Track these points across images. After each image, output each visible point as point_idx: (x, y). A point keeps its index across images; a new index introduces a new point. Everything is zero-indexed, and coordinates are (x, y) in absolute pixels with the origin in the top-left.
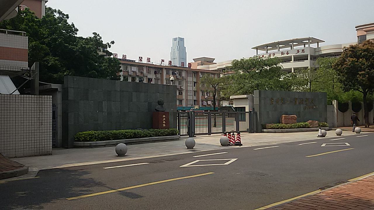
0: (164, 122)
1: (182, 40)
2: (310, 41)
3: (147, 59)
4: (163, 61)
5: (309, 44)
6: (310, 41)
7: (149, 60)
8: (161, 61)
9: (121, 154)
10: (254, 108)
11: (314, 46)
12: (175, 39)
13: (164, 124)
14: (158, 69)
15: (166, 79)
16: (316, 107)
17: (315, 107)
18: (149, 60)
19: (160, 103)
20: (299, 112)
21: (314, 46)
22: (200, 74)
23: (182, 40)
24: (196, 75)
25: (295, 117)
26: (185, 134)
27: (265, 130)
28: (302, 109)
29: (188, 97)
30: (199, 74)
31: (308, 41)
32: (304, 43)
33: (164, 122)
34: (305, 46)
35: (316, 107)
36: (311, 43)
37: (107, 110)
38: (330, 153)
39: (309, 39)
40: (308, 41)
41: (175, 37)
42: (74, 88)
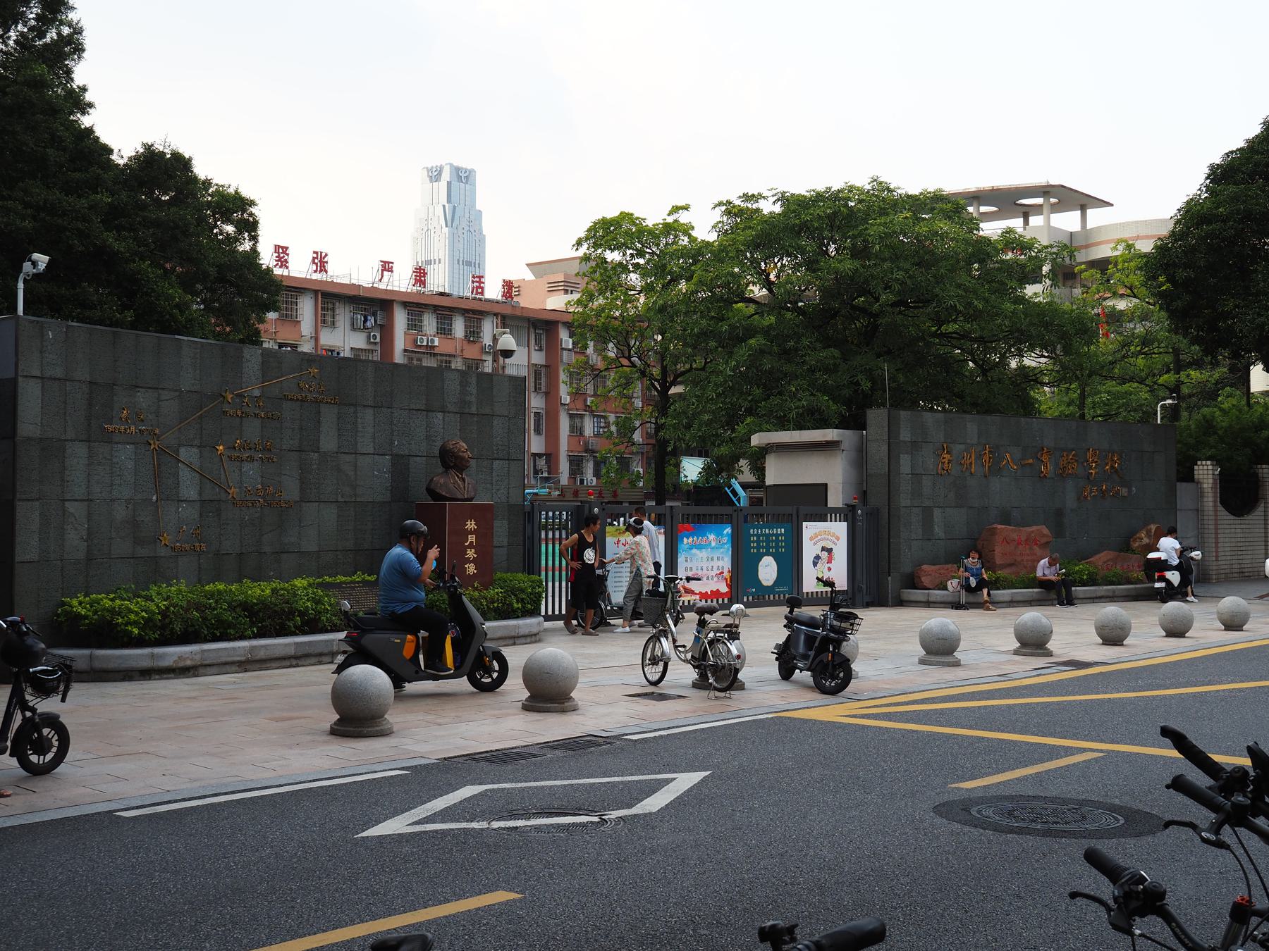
0: (471, 554)
1: (463, 177)
2: (1053, 200)
3: (312, 255)
4: (387, 267)
5: (1045, 210)
6: (1053, 200)
7: (320, 261)
8: (378, 266)
9: (355, 720)
10: (865, 492)
11: (1068, 221)
12: (435, 175)
13: (468, 561)
14: (371, 306)
15: (405, 350)
16: (1130, 491)
17: (1124, 491)
18: (320, 261)
19: (450, 461)
20: (1059, 513)
21: (1068, 221)
22: (564, 335)
23: (463, 177)
24: (544, 337)
25: (1044, 535)
26: (557, 612)
27: (918, 594)
28: (1070, 501)
29: (565, 437)
30: (558, 333)
31: (1039, 201)
32: (1025, 209)
33: (471, 554)
34: (1026, 222)
35: (1130, 491)
36: (1056, 209)
37: (200, 494)
38: (1159, 687)
39: (1045, 191)
40: (1039, 201)
41: (434, 162)
42: (42, 378)
